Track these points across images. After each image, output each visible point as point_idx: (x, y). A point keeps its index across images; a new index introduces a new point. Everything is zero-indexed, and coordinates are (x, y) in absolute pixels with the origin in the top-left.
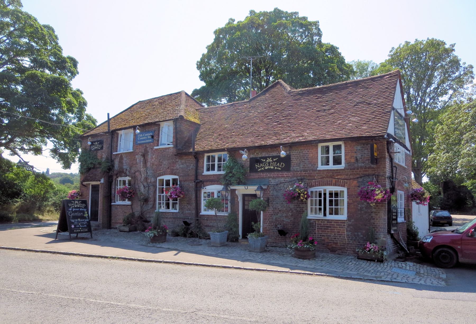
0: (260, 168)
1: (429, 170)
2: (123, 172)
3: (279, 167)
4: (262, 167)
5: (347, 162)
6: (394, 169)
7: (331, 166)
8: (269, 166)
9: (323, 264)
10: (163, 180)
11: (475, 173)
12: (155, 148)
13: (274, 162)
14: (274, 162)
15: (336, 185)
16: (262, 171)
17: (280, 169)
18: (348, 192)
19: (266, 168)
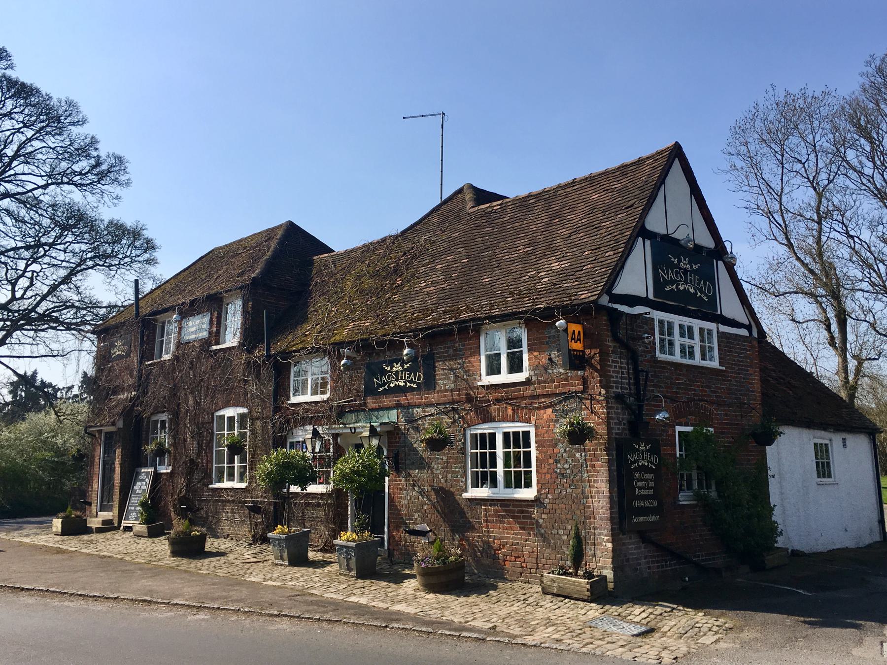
0: (381, 386)
1: (576, 645)
2: (371, 391)
3: (414, 383)
4: (384, 384)
5: (533, 368)
6: (642, 378)
7: (505, 377)
8: (397, 380)
9: (870, 91)
10: (224, 416)
11: (886, 408)
12: (215, 347)
13: (405, 370)
14: (405, 370)
15: (513, 421)
16: (385, 392)
17: (415, 386)
18: (537, 436)
19: (392, 385)
